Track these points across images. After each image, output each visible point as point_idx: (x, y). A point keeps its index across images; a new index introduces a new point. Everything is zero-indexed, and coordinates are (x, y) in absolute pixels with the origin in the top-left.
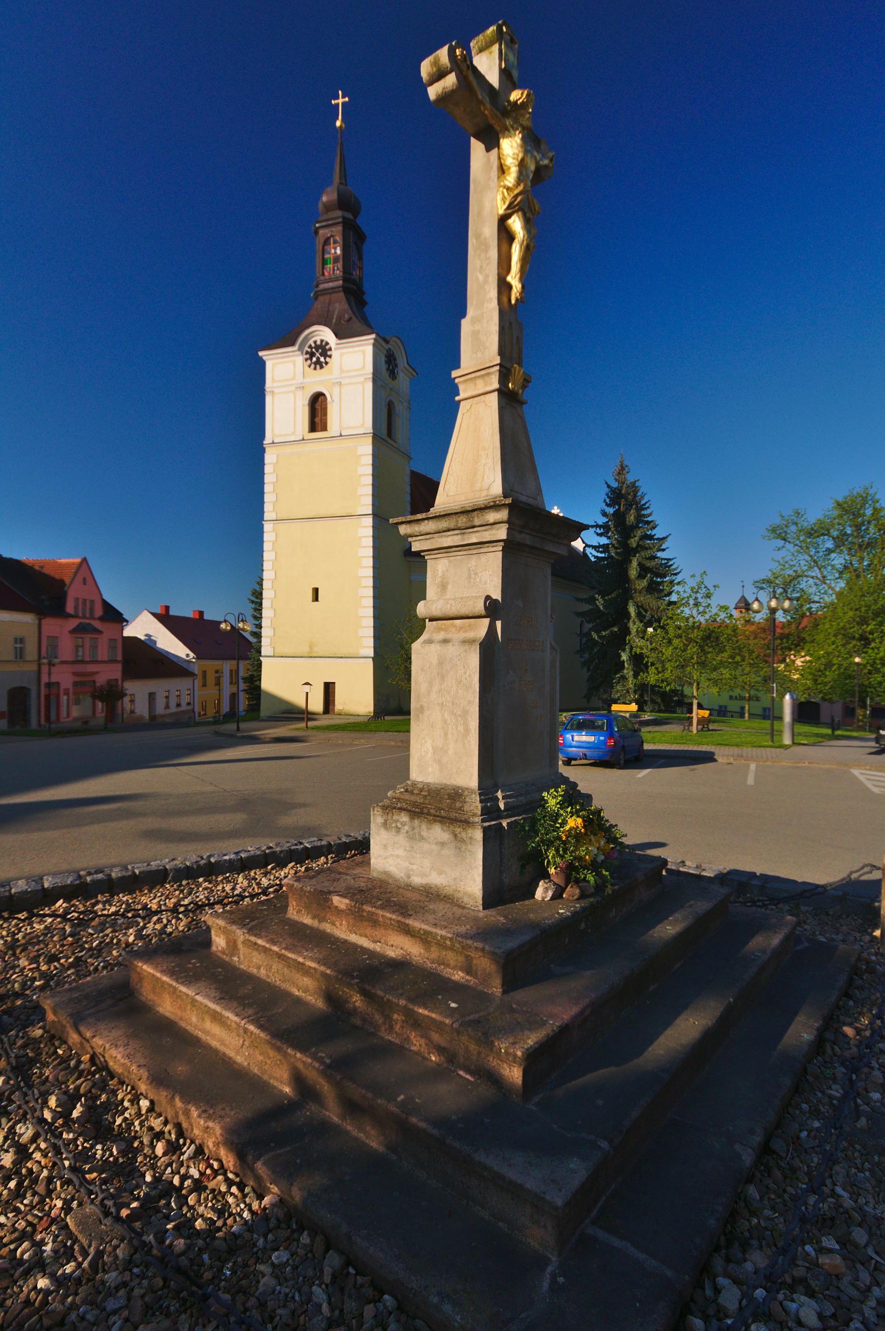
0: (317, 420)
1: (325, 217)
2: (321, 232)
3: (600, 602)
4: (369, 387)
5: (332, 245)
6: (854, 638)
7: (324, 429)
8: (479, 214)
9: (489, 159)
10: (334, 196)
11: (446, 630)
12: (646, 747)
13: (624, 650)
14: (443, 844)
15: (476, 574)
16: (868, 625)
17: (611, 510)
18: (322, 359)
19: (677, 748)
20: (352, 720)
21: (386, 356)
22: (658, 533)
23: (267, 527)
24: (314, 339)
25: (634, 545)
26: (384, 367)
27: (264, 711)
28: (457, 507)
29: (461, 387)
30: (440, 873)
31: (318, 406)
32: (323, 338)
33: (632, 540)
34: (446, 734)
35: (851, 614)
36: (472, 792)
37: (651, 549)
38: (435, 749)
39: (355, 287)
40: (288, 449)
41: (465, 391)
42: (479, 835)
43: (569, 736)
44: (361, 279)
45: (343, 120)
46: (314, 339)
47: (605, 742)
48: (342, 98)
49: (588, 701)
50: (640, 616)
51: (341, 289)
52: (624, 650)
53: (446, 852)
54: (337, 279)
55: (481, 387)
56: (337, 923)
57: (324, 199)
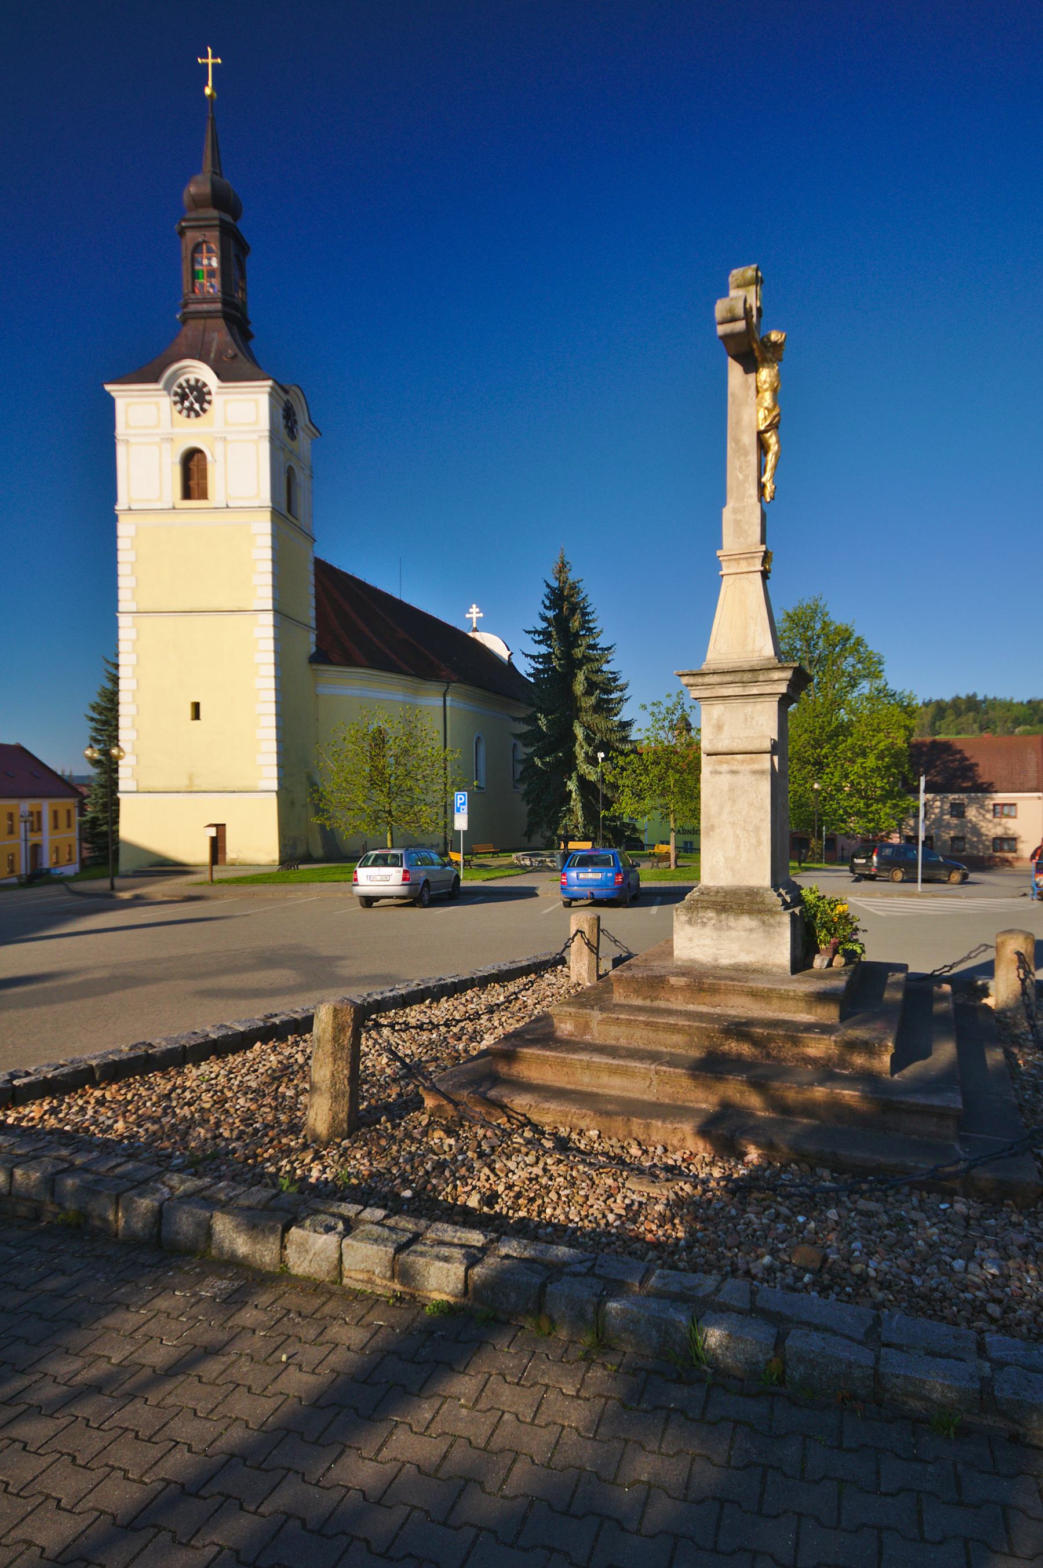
0: (193, 483)
1: (193, 215)
2: (189, 234)
3: (543, 722)
4: (265, 447)
5: (205, 254)
6: (808, 762)
7: (203, 495)
8: (738, 423)
9: (747, 380)
10: (207, 189)
11: (727, 763)
12: (642, 885)
13: (570, 778)
14: (751, 930)
15: (752, 718)
16: (822, 749)
17: (550, 614)
18: (197, 406)
19: (667, 885)
20: (252, 872)
21: (284, 410)
22: (603, 642)
23: (123, 621)
24: (186, 377)
25: (580, 656)
26: (282, 422)
27: (125, 864)
28: (746, 667)
29: (724, 564)
30: (749, 952)
31: (193, 465)
32: (198, 377)
33: (577, 650)
34: (738, 847)
35: (806, 736)
36: (767, 889)
37: (597, 660)
38: (727, 860)
39: (239, 315)
40: (151, 519)
41: (728, 567)
42: (786, 919)
43: (574, 874)
44: (244, 303)
45: (214, 88)
46: (186, 377)
47: (613, 879)
48: (207, 58)
49: (529, 840)
50: (588, 739)
51: (220, 314)
52: (570, 778)
53: (754, 936)
54: (213, 301)
55: (744, 566)
56: (672, 999)
57: (192, 189)
